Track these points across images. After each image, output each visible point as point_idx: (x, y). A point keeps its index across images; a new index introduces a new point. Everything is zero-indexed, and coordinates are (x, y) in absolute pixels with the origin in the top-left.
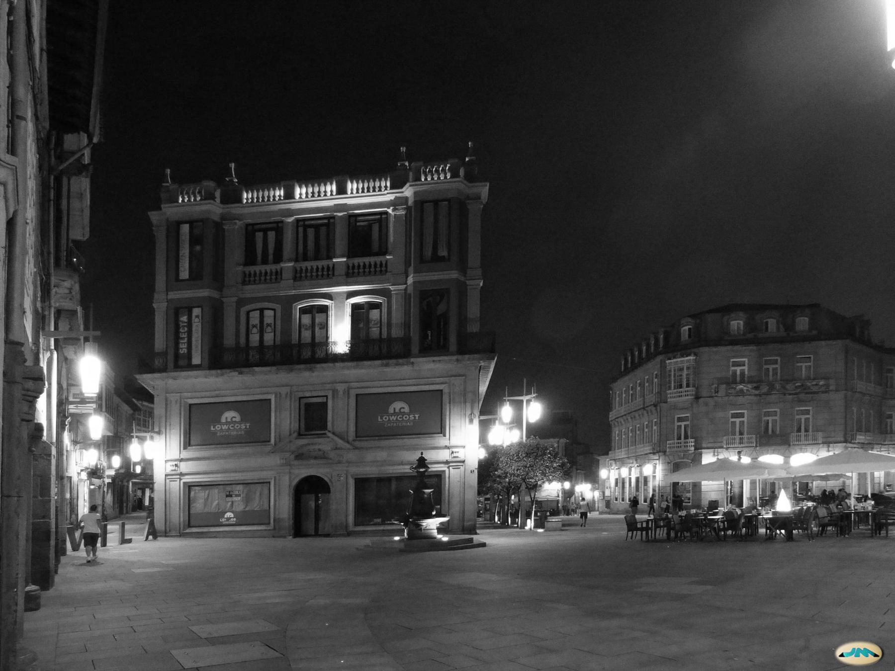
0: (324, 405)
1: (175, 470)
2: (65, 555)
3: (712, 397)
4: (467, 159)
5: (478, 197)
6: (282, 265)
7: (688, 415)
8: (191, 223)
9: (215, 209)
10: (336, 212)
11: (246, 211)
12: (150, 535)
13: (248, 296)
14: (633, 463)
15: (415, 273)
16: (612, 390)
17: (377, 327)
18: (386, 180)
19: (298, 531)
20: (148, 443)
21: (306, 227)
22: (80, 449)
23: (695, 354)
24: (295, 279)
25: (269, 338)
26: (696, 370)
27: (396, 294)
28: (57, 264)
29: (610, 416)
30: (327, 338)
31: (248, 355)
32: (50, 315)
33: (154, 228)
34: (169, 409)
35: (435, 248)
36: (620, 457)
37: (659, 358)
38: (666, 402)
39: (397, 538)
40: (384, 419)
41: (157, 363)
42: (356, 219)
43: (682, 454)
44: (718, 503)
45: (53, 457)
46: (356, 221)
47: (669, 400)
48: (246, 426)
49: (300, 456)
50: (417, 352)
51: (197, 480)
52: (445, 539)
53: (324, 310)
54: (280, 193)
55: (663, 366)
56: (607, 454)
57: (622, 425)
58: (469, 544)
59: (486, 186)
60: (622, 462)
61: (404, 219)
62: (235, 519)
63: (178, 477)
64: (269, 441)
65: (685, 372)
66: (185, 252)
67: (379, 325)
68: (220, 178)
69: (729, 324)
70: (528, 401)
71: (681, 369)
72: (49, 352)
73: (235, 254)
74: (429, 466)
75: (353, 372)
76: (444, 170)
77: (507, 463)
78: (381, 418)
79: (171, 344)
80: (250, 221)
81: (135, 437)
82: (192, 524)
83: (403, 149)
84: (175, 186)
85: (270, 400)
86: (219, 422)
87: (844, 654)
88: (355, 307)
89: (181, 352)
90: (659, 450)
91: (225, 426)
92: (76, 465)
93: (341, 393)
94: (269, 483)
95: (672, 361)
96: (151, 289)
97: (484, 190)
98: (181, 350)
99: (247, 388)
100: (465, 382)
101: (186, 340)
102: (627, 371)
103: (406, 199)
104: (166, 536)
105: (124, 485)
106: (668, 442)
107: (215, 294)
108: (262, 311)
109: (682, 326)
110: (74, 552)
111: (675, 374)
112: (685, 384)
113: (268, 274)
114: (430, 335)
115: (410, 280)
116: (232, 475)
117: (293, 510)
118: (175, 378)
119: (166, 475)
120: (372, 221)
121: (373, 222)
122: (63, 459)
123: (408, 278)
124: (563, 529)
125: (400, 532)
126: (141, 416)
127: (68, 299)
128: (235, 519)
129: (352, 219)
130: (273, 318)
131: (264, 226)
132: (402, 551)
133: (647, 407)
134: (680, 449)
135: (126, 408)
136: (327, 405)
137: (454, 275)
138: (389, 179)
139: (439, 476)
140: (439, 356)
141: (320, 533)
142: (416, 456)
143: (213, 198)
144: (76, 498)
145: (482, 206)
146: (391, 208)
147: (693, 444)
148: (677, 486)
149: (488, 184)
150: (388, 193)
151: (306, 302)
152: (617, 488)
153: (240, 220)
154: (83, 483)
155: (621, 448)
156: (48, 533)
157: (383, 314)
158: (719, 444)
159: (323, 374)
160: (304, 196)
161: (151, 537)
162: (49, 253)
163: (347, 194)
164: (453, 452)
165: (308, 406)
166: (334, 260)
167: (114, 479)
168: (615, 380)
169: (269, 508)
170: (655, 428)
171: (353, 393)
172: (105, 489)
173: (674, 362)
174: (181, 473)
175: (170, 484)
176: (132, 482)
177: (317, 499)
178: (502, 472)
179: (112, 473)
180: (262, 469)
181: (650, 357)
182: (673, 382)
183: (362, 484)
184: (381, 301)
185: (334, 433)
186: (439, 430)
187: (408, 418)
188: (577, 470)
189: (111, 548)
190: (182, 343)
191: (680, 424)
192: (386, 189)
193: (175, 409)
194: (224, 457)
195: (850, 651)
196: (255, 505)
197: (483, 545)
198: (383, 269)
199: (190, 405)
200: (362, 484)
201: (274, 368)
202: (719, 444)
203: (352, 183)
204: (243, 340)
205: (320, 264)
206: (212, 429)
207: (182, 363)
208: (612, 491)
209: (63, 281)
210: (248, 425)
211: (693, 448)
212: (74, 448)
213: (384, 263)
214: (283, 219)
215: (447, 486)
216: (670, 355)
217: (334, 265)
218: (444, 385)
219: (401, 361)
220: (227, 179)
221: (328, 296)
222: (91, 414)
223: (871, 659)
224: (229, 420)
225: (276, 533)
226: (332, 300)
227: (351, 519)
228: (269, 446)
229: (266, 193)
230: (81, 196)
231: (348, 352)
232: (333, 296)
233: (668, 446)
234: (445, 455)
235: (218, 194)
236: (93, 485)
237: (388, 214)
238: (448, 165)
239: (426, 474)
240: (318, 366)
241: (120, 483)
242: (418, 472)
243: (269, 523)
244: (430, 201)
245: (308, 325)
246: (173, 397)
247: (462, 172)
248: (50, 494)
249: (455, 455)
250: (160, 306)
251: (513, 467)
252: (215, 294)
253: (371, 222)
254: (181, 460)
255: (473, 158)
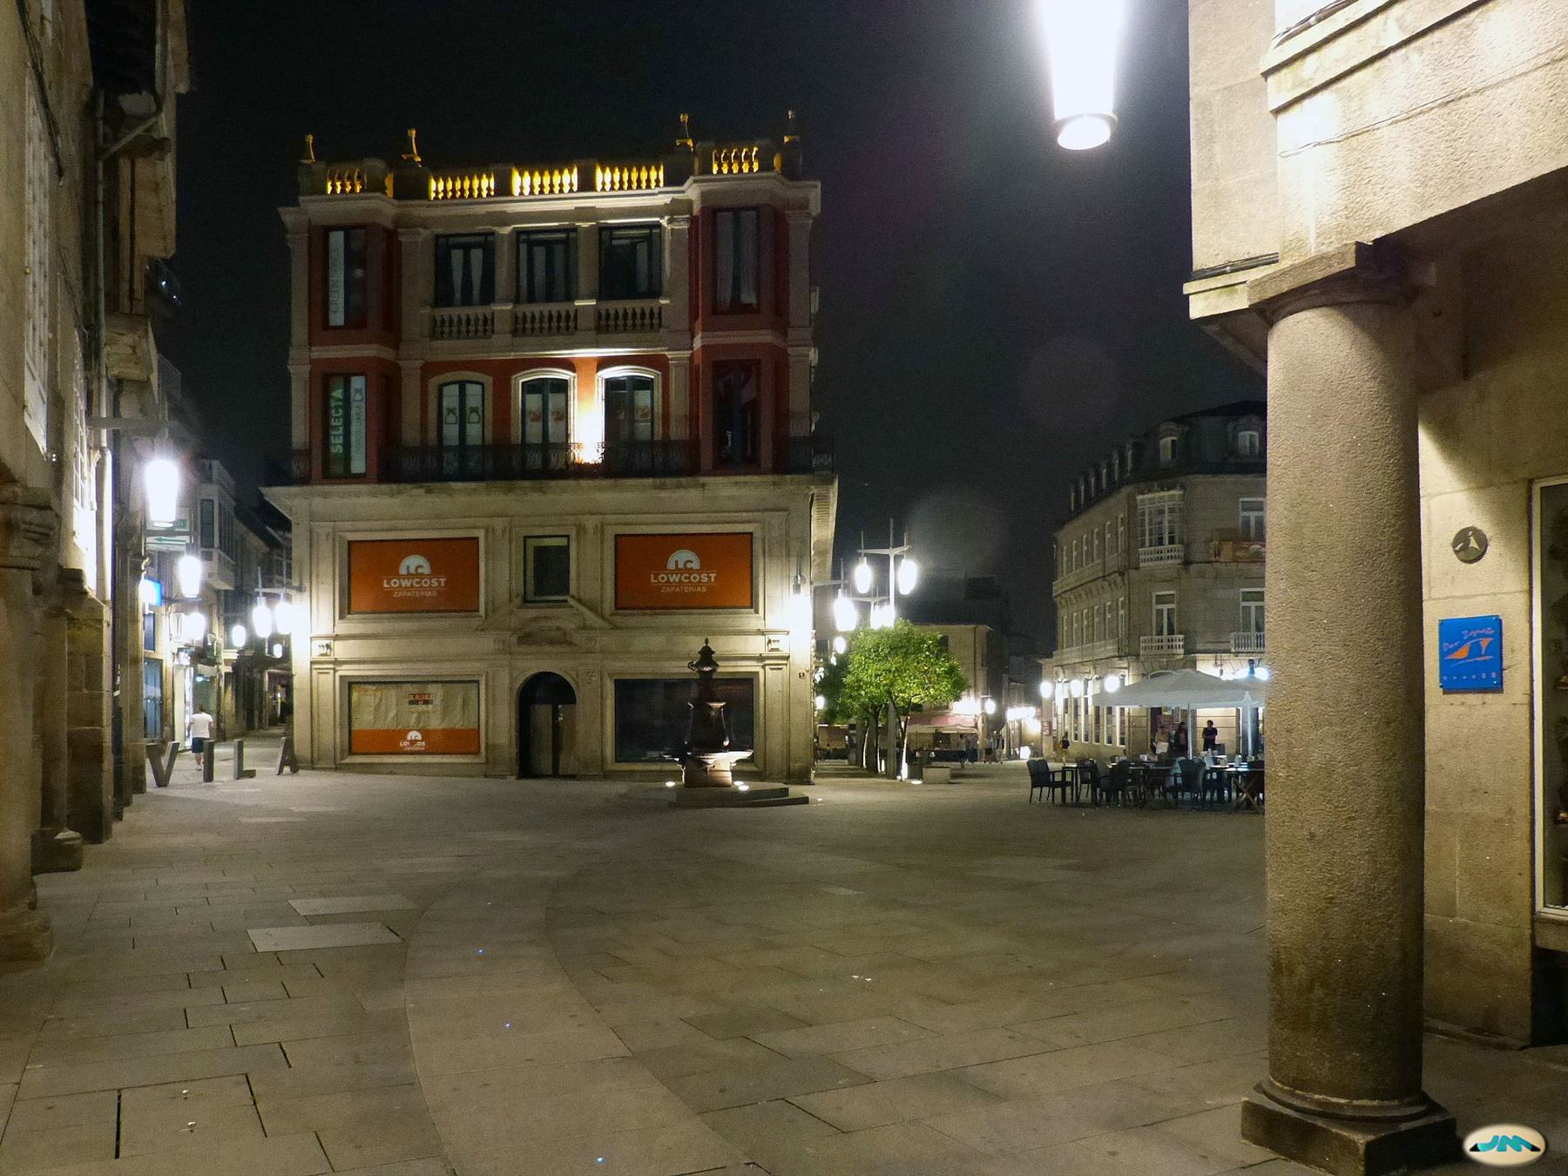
0: (564, 551)
1: (326, 655)
2: (143, 793)
3: (1210, 562)
4: (786, 140)
5: (804, 205)
6: (494, 308)
7: (1172, 592)
8: (347, 229)
9: (385, 206)
10: (579, 220)
11: (438, 212)
12: (287, 765)
13: (441, 358)
14: (1089, 673)
15: (703, 331)
16: (1056, 544)
17: (647, 421)
18: (658, 169)
19: (526, 768)
20: (281, 605)
21: (531, 244)
22: (177, 611)
23: (1183, 487)
24: (515, 332)
25: (474, 431)
26: (1184, 513)
27: (676, 366)
28: (113, 307)
29: (1054, 588)
30: (567, 436)
31: (440, 460)
32: (99, 389)
33: (288, 236)
34: (315, 552)
35: (736, 288)
36: (1070, 662)
37: (1126, 490)
38: (1137, 568)
39: (670, 784)
40: (423, 584)
41: (294, 468)
42: (611, 235)
43: (1165, 660)
44: (1224, 748)
45: (105, 625)
46: (612, 238)
47: (1141, 565)
48: (439, 582)
49: (526, 638)
50: (710, 467)
51: (362, 673)
52: (742, 786)
53: (561, 387)
54: (487, 183)
55: (1132, 506)
56: (1050, 656)
57: (1072, 604)
58: (781, 798)
59: (816, 187)
60: (1073, 670)
61: (687, 236)
62: (424, 743)
63: (332, 666)
64: (478, 611)
65: (1167, 517)
66: (337, 277)
67: (649, 418)
68: (394, 155)
69: (1235, 437)
70: (898, 558)
71: (1161, 512)
72: (98, 451)
73: (418, 282)
74: (719, 663)
75: (609, 496)
76: (748, 157)
77: (861, 664)
78: (388, 583)
79: (319, 435)
80: (440, 231)
81: (261, 594)
82: (354, 749)
83: (684, 118)
84: (322, 165)
85: (477, 539)
86: (397, 574)
87: (1479, 1147)
88: (611, 385)
89: (334, 450)
90: (1128, 651)
91: (406, 580)
92: (171, 639)
93: (590, 531)
94: (477, 682)
95: (1145, 496)
96: (286, 343)
97: (813, 194)
98: (332, 447)
99: (438, 517)
100: (787, 521)
101: (341, 431)
102: (1080, 510)
103: (690, 203)
104: (313, 769)
105: (254, 679)
106: (1141, 638)
107: (387, 354)
108: (462, 384)
109: (1161, 436)
110: (160, 789)
111: (1151, 520)
112: (1166, 537)
113: (472, 323)
114: (729, 438)
115: (698, 343)
116: (419, 665)
117: (516, 732)
118: (325, 495)
119: (312, 663)
120: (638, 238)
121: (639, 240)
122: (138, 627)
123: (695, 339)
124: (951, 781)
125: (674, 775)
126: (282, 557)
127: (133, 363)
128: (424, 743)
129: (605, 235)
130: (480, 398)
131: (464, 240)
132: (673, 806)
133: (1109, 575)
134: (1162, 652)
135: (254, 542)
136: (568, 553)
137: (765, 337)
138: (662, 167)
139: (749, 681)
140: (745, 474)
141: (561, 771)
142: (697, 644)
143: (383, 189)
144: (171, 697)
145: (811, 221)
146: (667, 218)
147: (1181, 643)
148: (1159, 716)
149: (819, 184)
150: (660, 193)
151: (533, 373)
152: (1066, 715)
153: (425, 227)
154: (182, 672)
155: (1072, 646)
156: (98, 750)
157: (655, 400)
158: (1223, 646)
159: (565, 497)
160: (527, 191)
161: (287, 769)
162: (97, 289)
163: (596, 191)
164: (770, 641)
165: (540, 551)
166: (577, 303)
167: (236, 666)
168: (1061, 524)
169: (479, 726)
170: (1122, 612)
171: (611, 532)
172: (222, 684)
173: (1150, 499)
174: (336, 659)
175: (318, 678)
176: (269, 673)
177: (555, 713)
178: (853, 678)
179: (233, 656)
180: (461, 658)
181: (1114, 488)
182: (1147, 534)
183: (628, 691)
184: (653, 377)
185: (579, 601)
186: (749, 605)
187: (698, 579)
188: (1011, 680)
189: (220, 784)
190: (335, 435)
191: (1160, 607)
192: (657, 185)
193: (325, 549)
194: (402, 635)
195: (1489, 1141)
196: (457, 721)
197: (805, 801)
198: (656, 321)
199: (350, 543)
200: (628, 691)
201: (482, 485)
202: (1223, 646)
203: (603, 171)
204: (432, 435)
205: (554, 308)
206: (386, 586)
207: (334, 472)
208: (1060, 721)
209: (123, 334)
210: (713, 575)
211: (1182, 651)
212: (167, 610)
213: (656, 311)
214: (494, 228)
215: (762, 698)
216: (1142, 485)
217: (576, 310)
218: (755, 525)
219: (683, 480)
220: (403, 156)
221: (568, 364)
222: (183, 553)
223: (1526, 1156)
224: (412, 571)
225: (489, 770)
226: (574, 371)
227: (609, 751)
228: (478, 619)
229: (476, 183)
230: (156, 188)
231: (600, 461)
232: (575, 363)
233: (1142, 645)
234: (757, 646)
235: (389, 182)
236: (201, 675)
237: (663, 229)
238: (755, 149)
239: (715, 676)
240: (553, 483)
241: (247, 674)
242: (701, 672)
243: (477, 753)
244: (727, 209)
245: (538, 413)
246: (323, 528)
247: (777, 162)
248: (101, 686)
249: (773, 646)
250: (298, 374)
251: (870, 671)
252: (387, 354)
253: (636, 240)
254: (337, 638)
255: (797, 138)
